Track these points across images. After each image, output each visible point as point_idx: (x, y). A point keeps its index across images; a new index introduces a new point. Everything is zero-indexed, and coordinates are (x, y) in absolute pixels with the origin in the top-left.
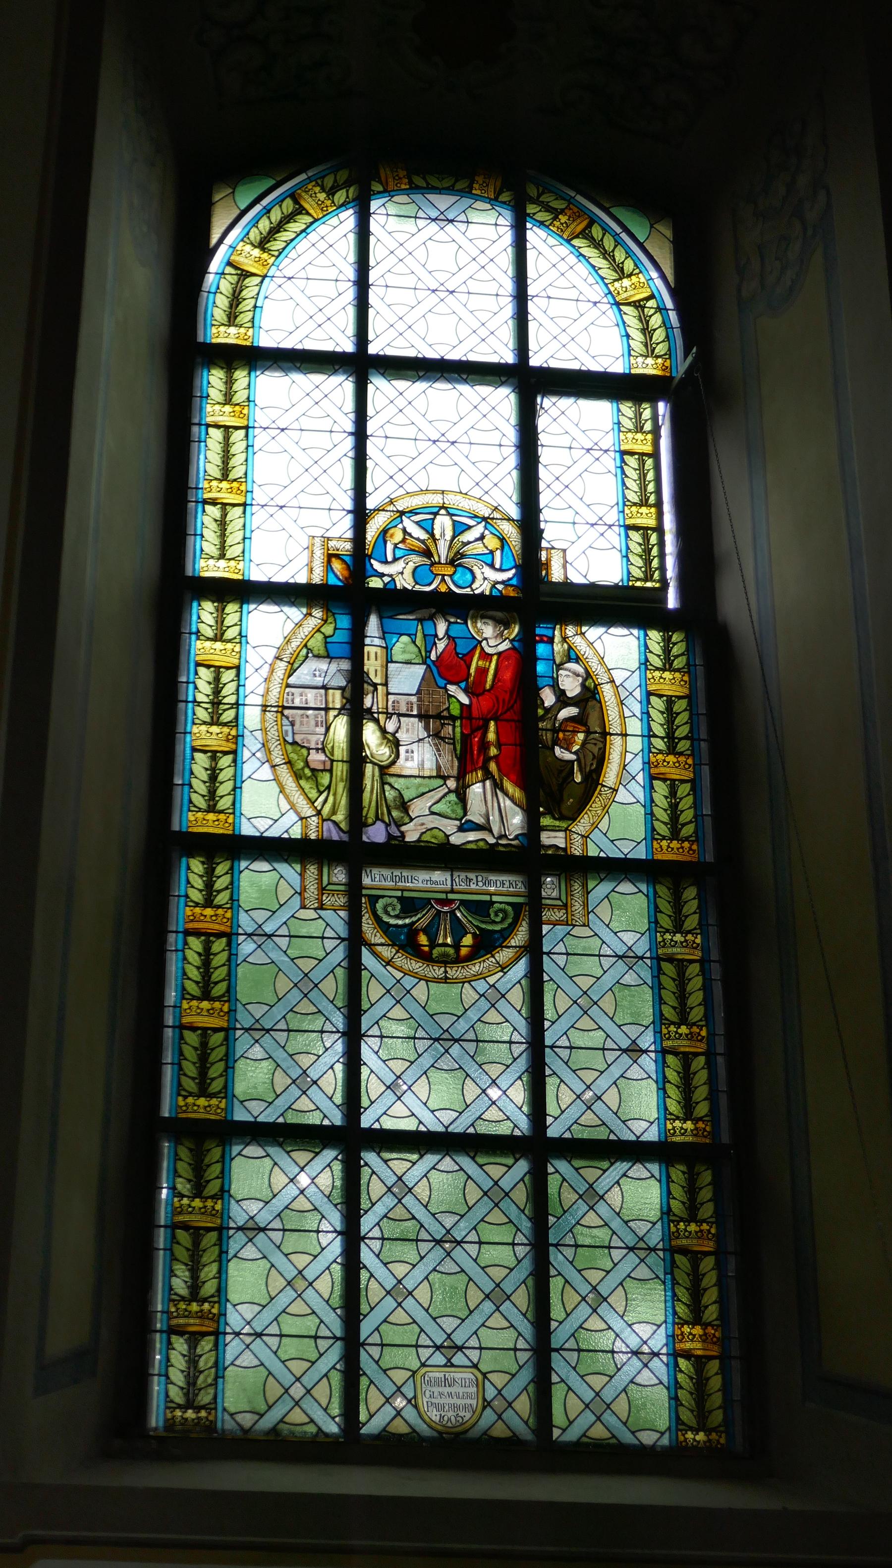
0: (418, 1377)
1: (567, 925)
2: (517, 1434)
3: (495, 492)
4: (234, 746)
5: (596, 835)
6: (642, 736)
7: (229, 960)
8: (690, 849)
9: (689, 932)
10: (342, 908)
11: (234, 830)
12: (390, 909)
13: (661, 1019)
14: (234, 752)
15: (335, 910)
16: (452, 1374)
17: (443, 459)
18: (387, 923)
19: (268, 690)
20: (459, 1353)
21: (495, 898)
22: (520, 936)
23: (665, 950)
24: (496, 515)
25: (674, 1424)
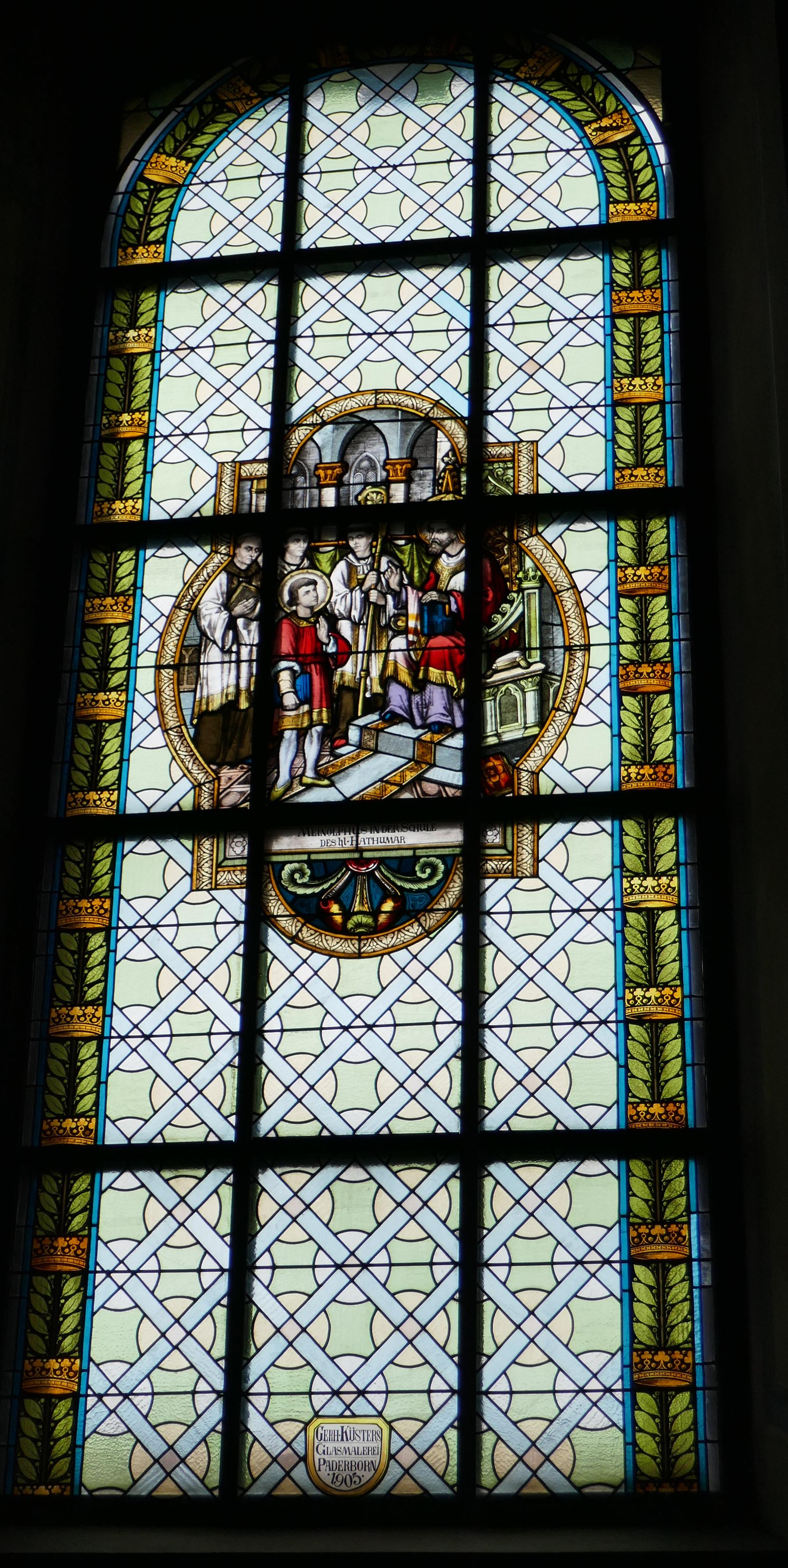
0: (311, 1429)
1: (513, 877)
2: (428, 1488)
3: (438, 386)
4: (130, 617)
5: (551, 768)
6: (610, 644)
7: (129, 648)
8: (655, 384)
9: (664, 874)
10: (240, 885)
11: (141, 516)
12: (297, 876)
13: (620, 760)
14: (130, 624)
15: (231, 889)
16: (352, 1426)
17: (384, 186)
18: (294, 894)
19: (163, 645)
20: (361, 1398)
21: (419, 853)
22: (455, 887)
23: (635, 1010)
24: (437, 413)
25: (627, 1343)
